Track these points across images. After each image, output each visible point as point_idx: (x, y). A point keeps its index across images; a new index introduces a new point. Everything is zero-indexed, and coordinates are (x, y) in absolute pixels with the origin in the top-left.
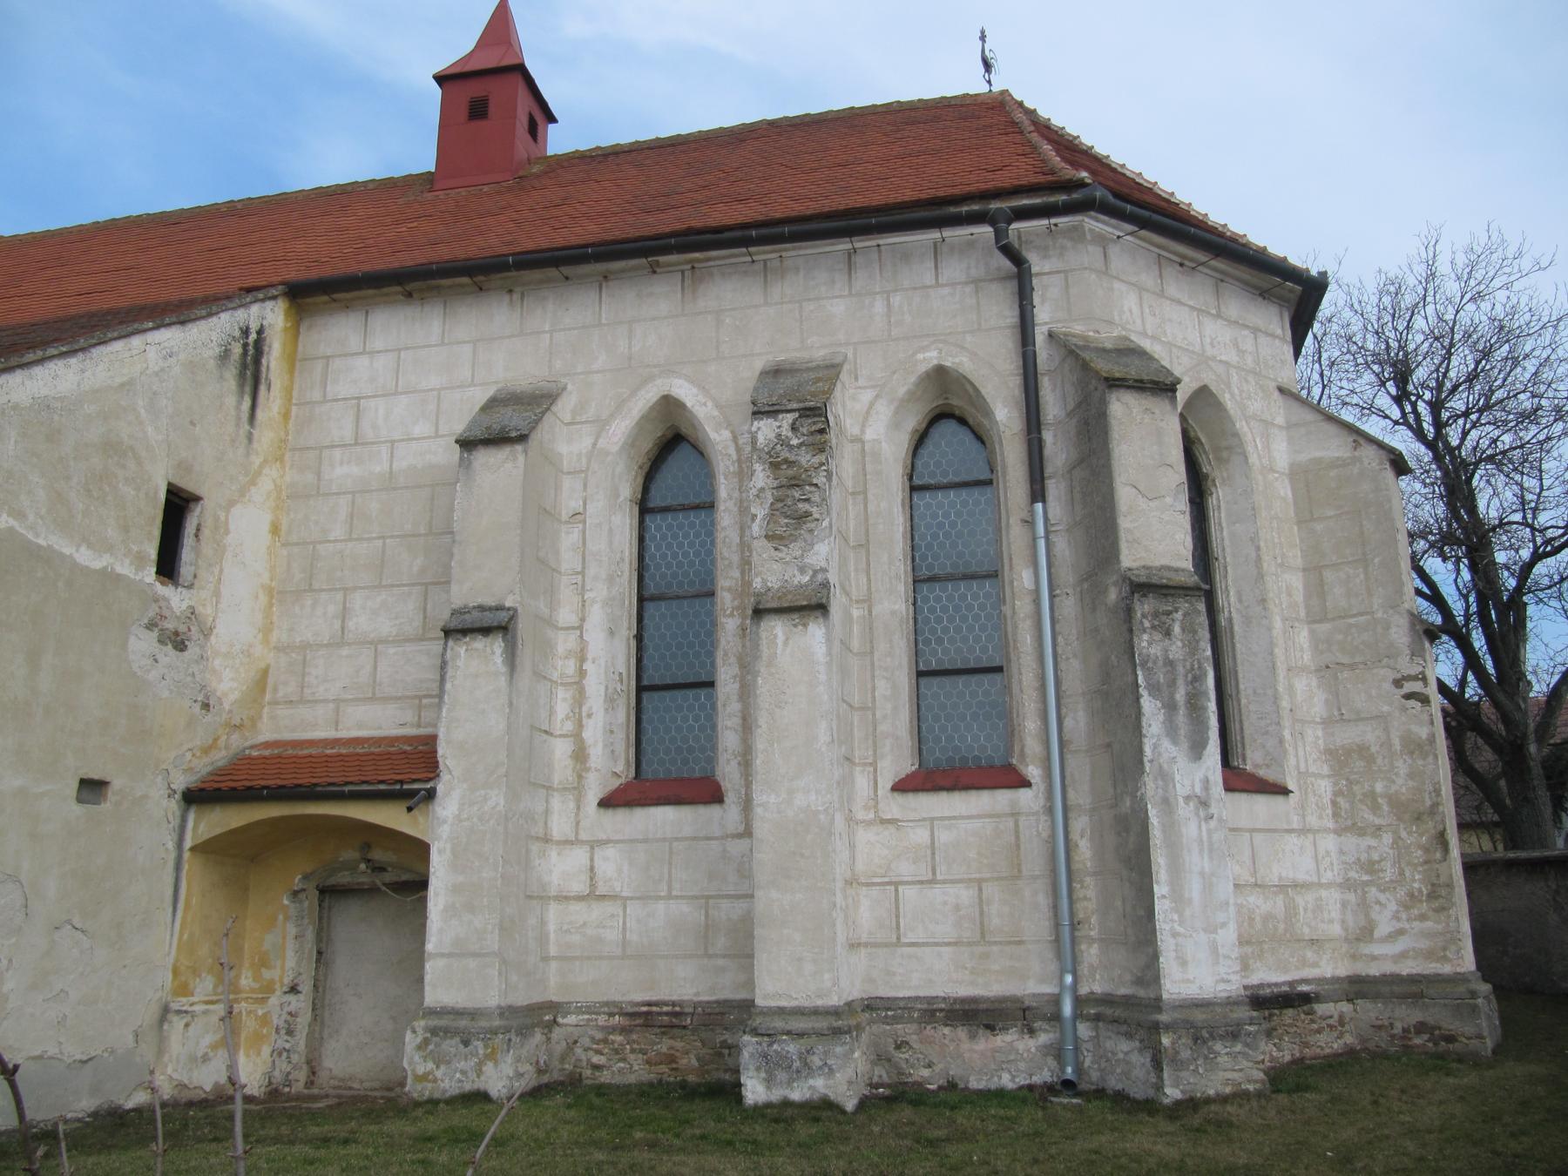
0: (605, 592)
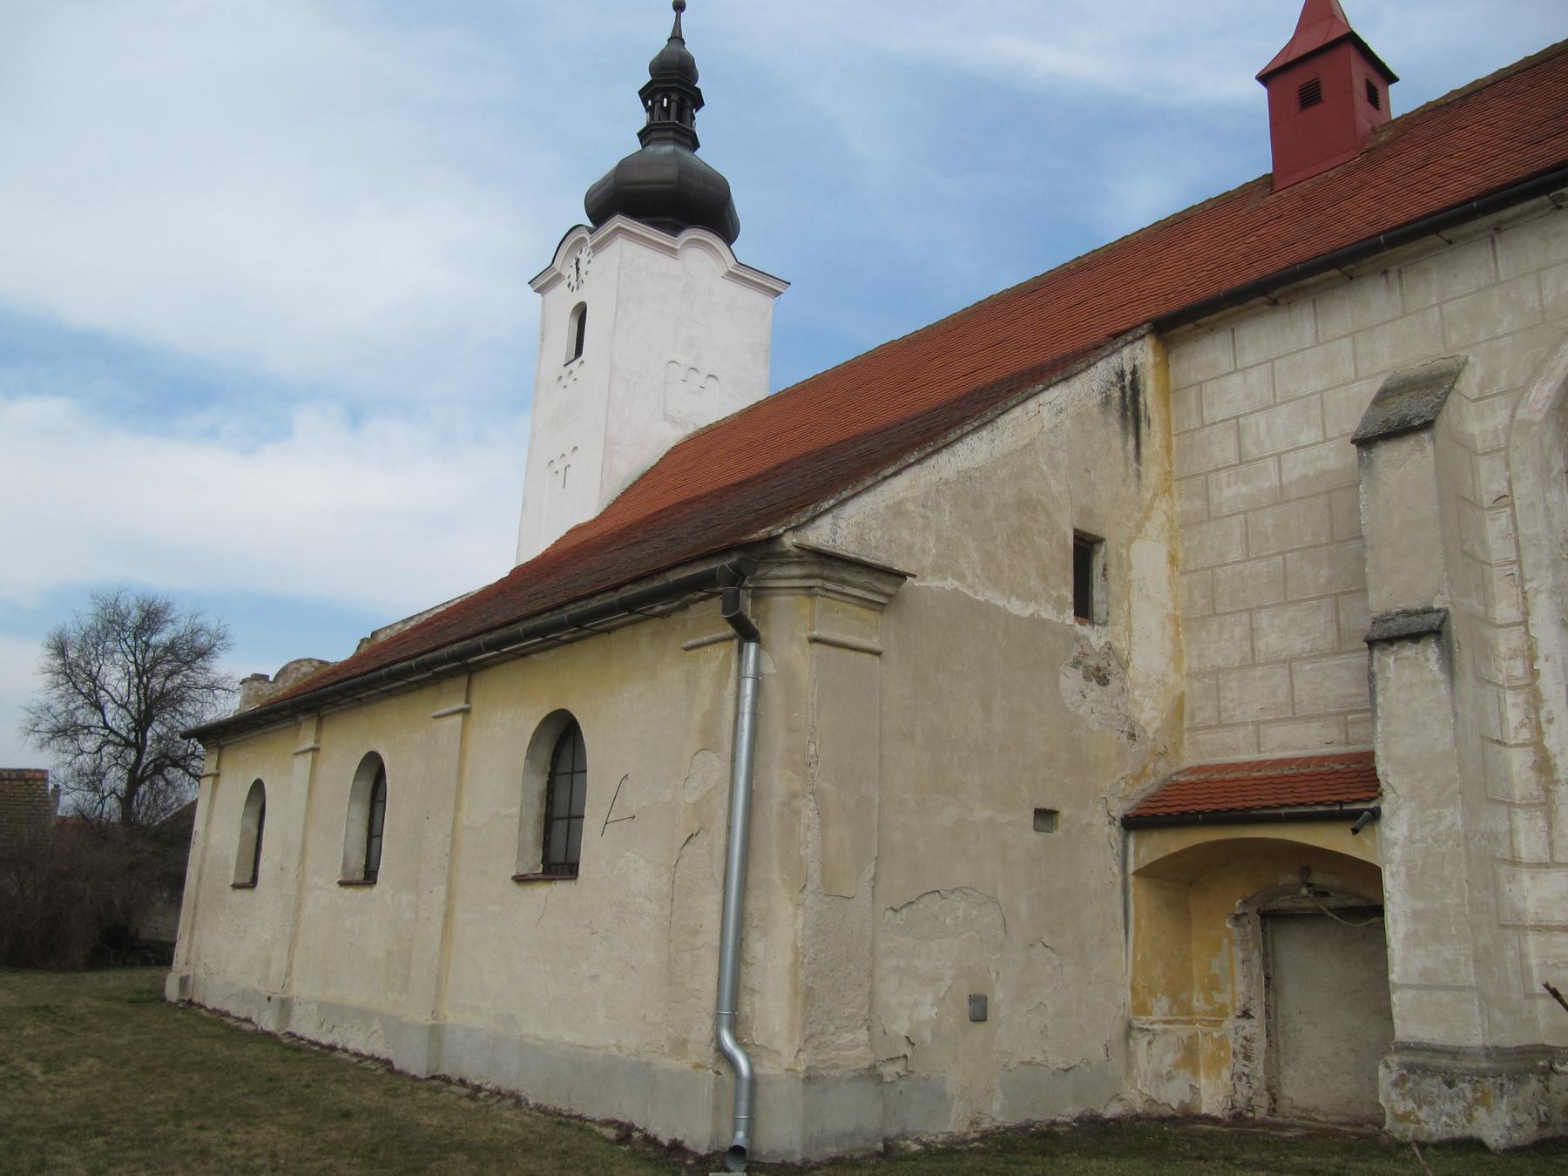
0: (1550, 580)
